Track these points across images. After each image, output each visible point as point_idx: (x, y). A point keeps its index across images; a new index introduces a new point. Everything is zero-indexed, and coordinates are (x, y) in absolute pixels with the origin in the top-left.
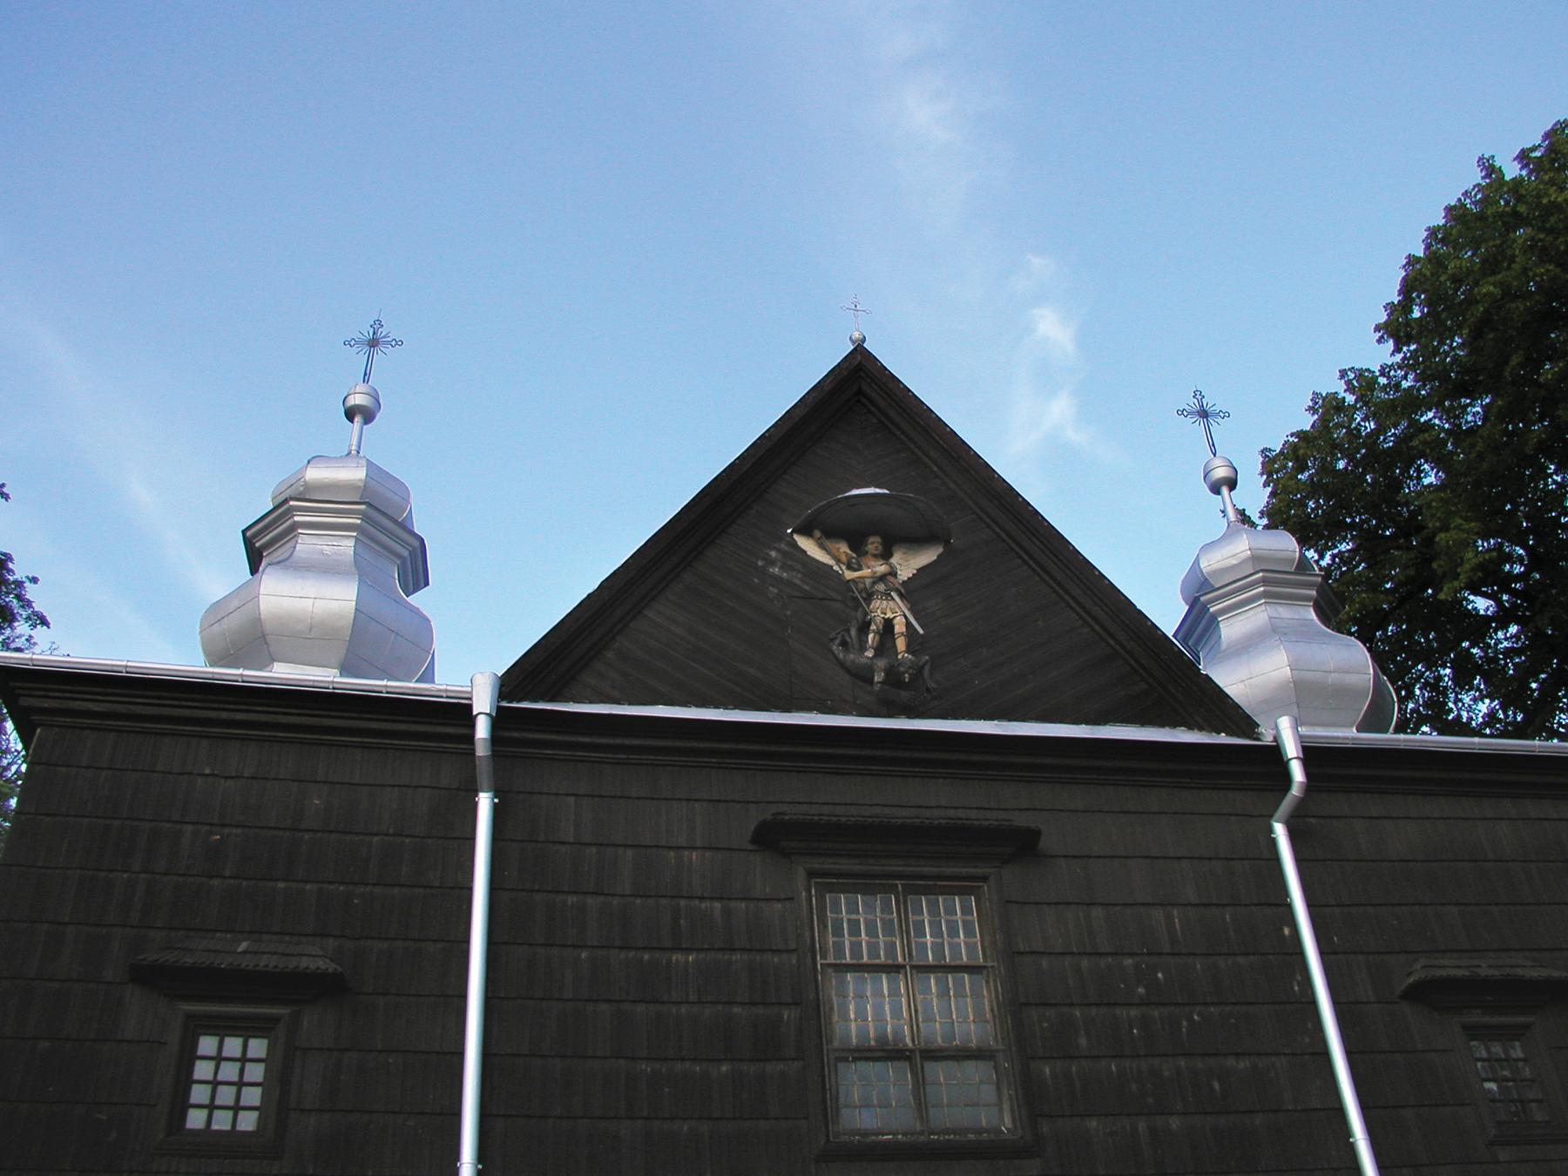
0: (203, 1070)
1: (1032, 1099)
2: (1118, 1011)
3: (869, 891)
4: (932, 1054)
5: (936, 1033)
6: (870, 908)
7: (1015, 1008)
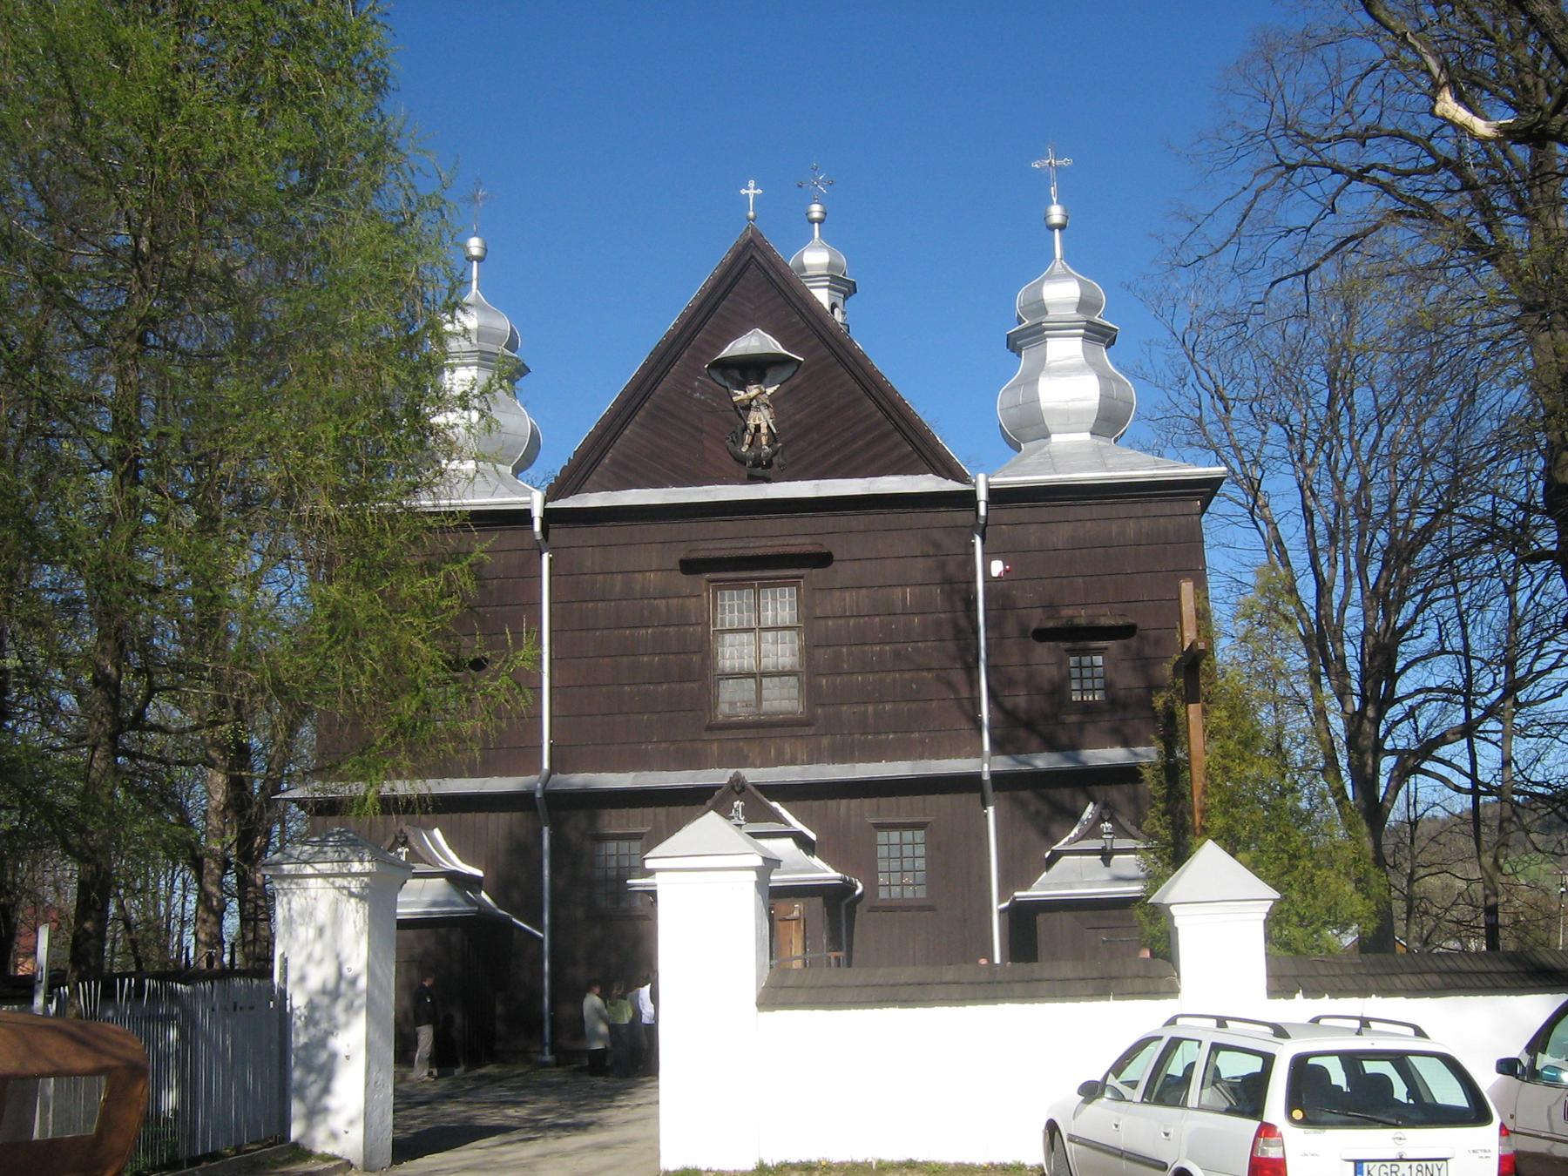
1: (811, 693)
2: (867, 648)
3: (741, 588)
4: (765, 674)
5: (768, 663)
6: (740, 598)
7: (808, 651)
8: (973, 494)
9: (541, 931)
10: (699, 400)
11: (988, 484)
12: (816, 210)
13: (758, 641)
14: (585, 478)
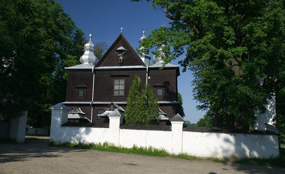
0: (158, 92)
3: (118, 79)
5: (120, 89)
6: (117, 80)
8: (146, 68)
9: (91, 121)
10: (114, 56)
11: (148, 67)
12: (144, 32)
13: (119, 86)
14: (100, 65)
